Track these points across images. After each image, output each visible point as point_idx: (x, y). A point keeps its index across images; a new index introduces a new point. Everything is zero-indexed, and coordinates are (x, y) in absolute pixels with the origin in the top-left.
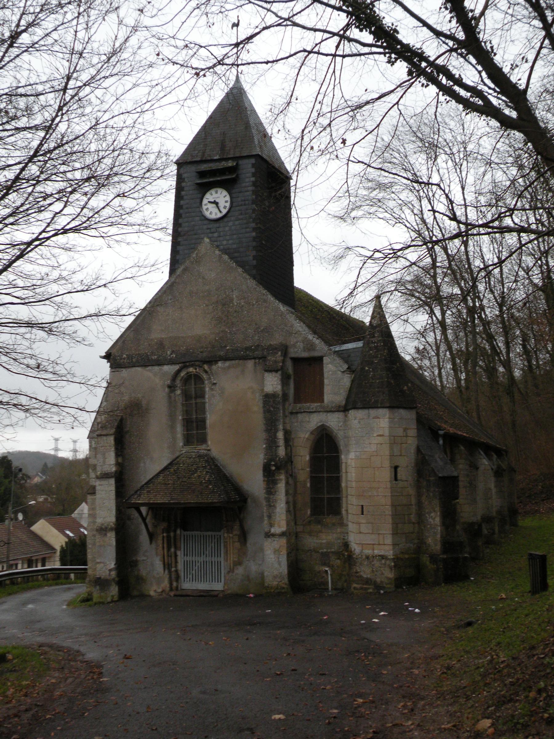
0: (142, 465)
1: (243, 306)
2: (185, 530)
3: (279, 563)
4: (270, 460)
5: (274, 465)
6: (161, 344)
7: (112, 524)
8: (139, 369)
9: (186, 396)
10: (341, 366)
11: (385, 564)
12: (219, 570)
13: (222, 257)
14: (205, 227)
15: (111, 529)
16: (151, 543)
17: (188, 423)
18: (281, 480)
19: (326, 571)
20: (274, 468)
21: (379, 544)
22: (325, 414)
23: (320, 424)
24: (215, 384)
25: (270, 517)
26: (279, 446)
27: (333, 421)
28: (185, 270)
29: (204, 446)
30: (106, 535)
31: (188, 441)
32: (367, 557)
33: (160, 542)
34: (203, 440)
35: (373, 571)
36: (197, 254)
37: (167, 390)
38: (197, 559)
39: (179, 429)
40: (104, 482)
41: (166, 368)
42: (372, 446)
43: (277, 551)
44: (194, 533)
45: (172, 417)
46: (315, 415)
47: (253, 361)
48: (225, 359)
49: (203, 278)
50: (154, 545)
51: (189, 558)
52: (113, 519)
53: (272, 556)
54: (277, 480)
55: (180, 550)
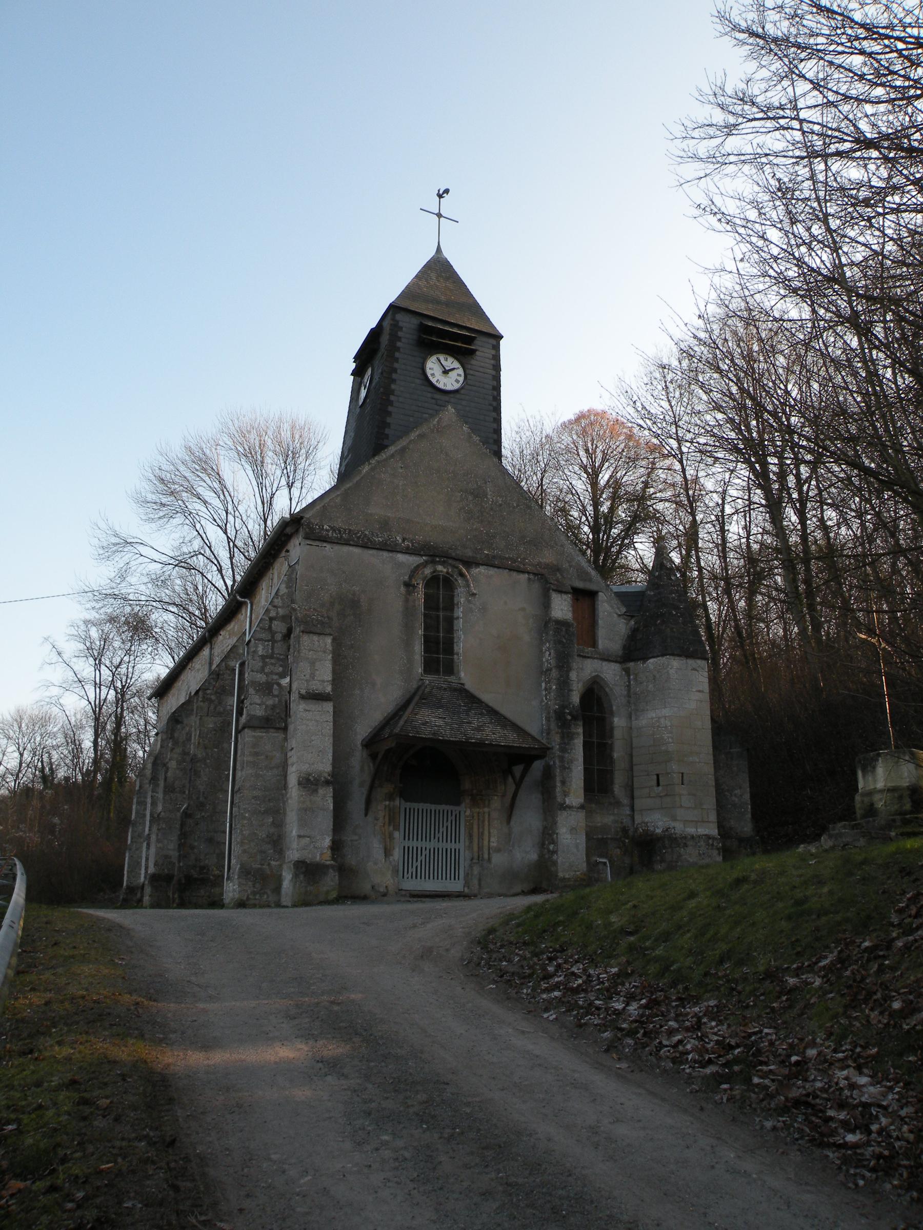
0: (357, 692)
1: (501, 505)
2: (406, 801)
3: (577, 846)
4: (563, 707)
5: (570, 714)
6: (385, 524)
7: (326, 775)
8: (356, 550)
9: (431, 603)
10: (618, 608)
11: (713, 845)
12: (457, 863)
13: (471, 437)
14: (401, 399)
15: (327, 783)
16: (366, 815)
17: (430, 644)
18: (578, 734)
19: (605, 863)
20: (569, 717)
21: (703, 822)
22: (600, 662)
23: (594, 674)
24: (474, 595)
25: (563, 783)
26: (572, 690)
27: (611, 673)
28: (422, 436)
29: (452, 679)
30: (316, 791)
31: (430, 666)
32: (693, 837)
33: (381, 814)
34: (450, 669)
35: (700, 854)
36: (438, 422)
37: (403, 589)
38: (424, 844)
39: (418, 648)
40: (314, 706)
41: (401, 557)
42: (676, 705)
43: (573, 830)
44: (421, 806)
45: (408, 628)
46: (589, 661)
47: (527, 575)
48: (489, 564)
49: (447, 455)
50: (370, 818)
51: (414, 844)
52: (328, 768)
53: (569, 836)
54: (574, 734)
55: (399, 830)
